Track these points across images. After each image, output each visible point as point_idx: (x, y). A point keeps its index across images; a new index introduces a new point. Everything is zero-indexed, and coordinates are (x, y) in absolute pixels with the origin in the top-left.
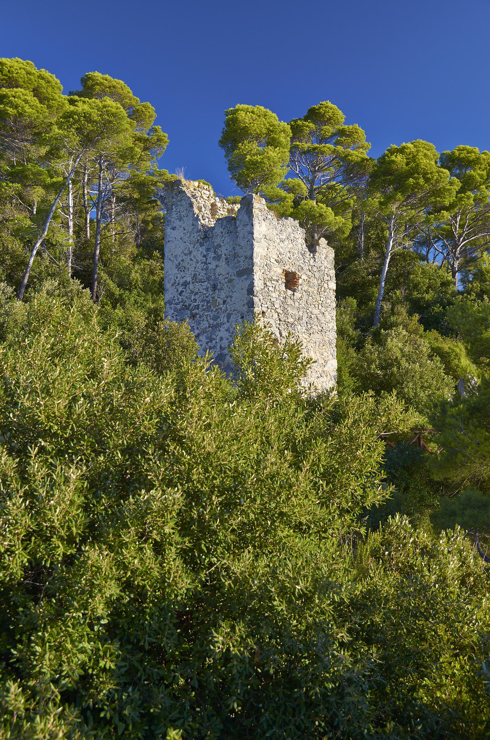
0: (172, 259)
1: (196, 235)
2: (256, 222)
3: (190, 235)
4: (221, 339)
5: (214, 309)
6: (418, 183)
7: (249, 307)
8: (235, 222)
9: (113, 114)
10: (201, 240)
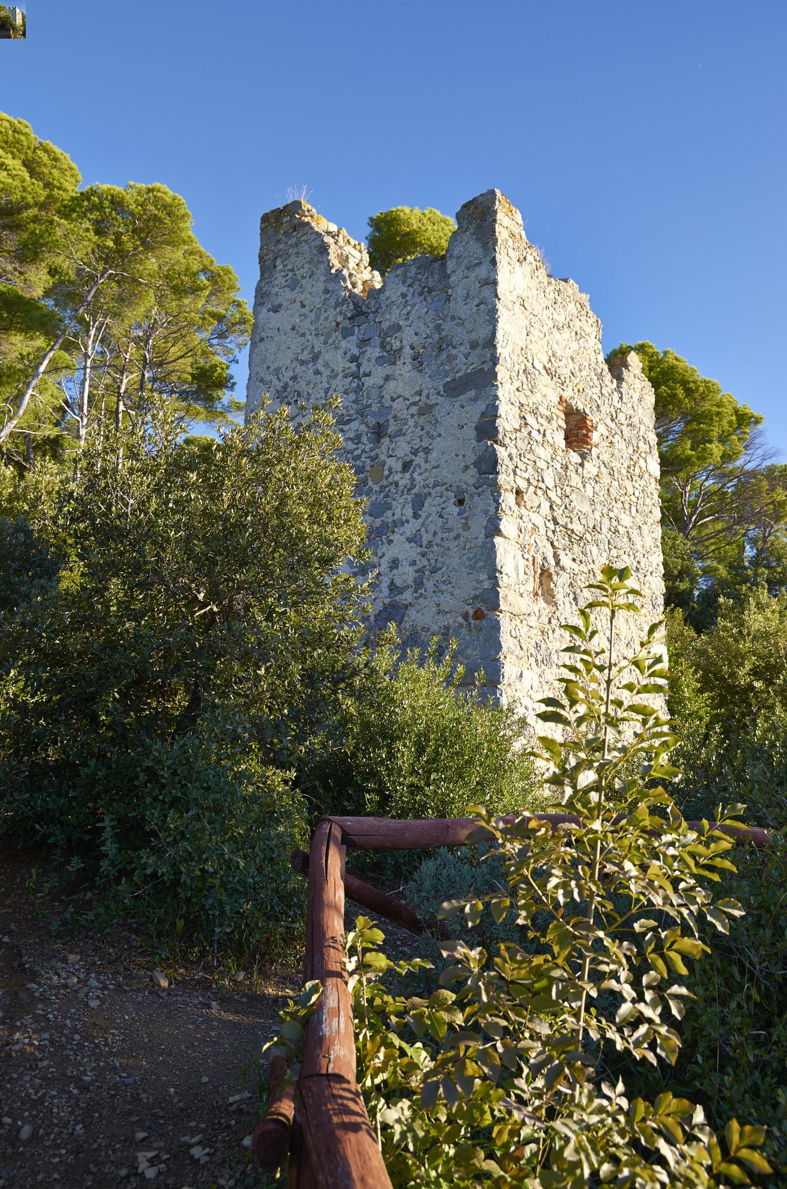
0: (268, 378)
1: (332, 313)
2: (501, 257)
3: (318, 317)
4: (395, 564)
5: (376, 488)
6: (674, 396)
7: (481, 473)
8: (444, 266)
9: (165, 206)
10: (347, 323)
